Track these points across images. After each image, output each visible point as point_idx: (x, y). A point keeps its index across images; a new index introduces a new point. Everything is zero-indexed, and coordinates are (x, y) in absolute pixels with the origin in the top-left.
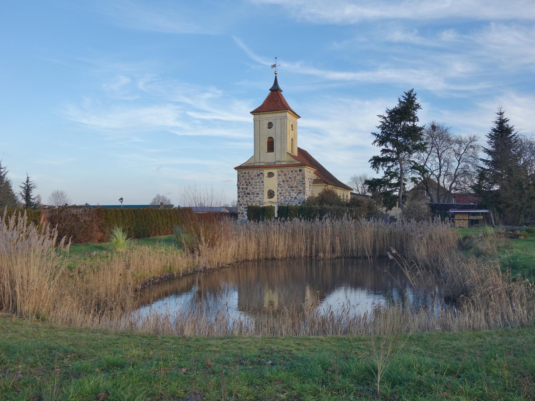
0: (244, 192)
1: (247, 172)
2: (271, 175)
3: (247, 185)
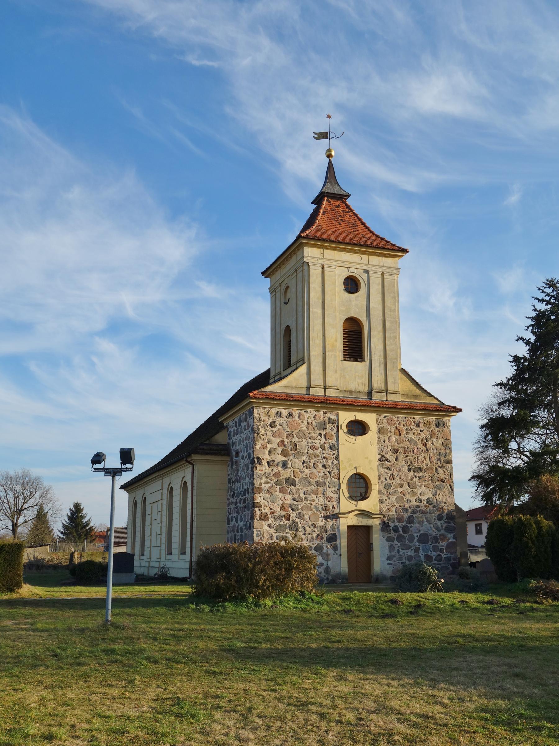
0: (277, 475)
1: (285, 412)
2: (358, 428)
3: (284, 453)
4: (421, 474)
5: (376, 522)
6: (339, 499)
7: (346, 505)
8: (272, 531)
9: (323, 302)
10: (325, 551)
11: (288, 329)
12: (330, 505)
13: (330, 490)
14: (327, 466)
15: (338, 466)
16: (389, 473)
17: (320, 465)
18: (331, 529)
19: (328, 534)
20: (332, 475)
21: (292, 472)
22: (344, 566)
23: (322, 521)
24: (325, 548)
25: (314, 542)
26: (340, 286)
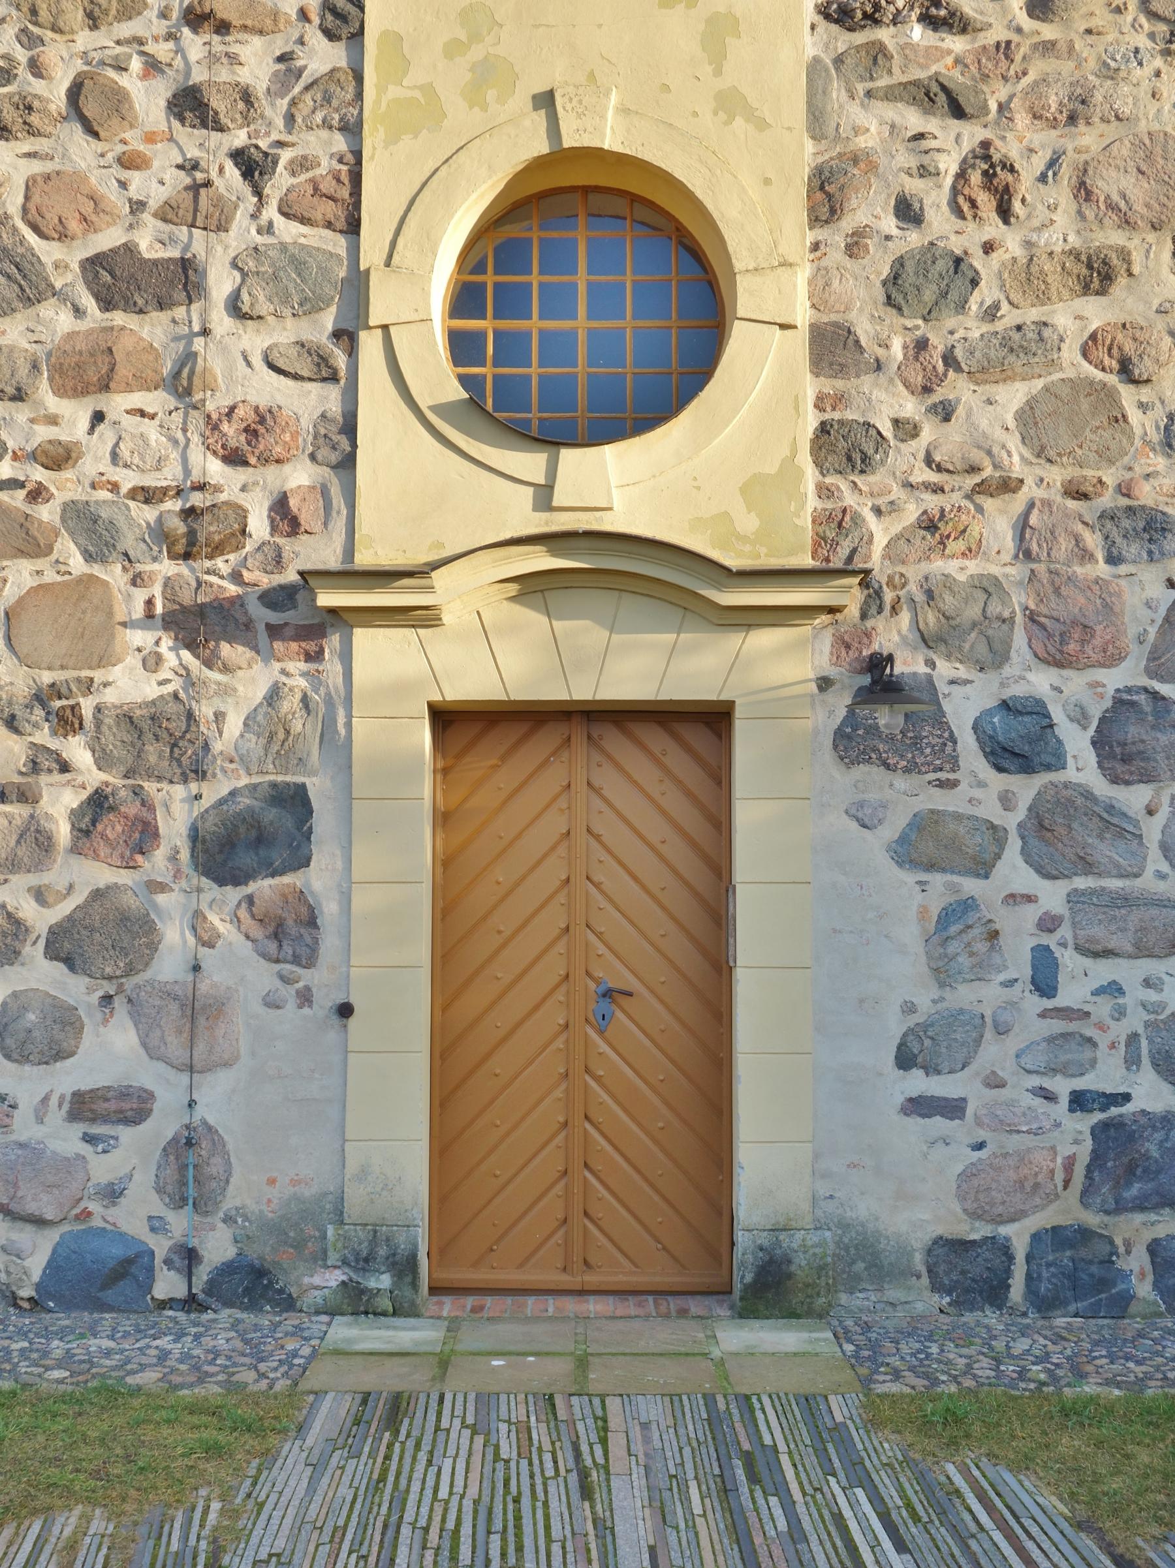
5: (776, 670)
6: (350, 428)
7: (432, 492)
10: (168, 966)
12: (249, 495)
13: (255, 341)
14: (217, 103)
16: (953, 144)
17: (149, 100)
18: (254, 744)
19: (214, 791)
20: (280, 183)
22: (390, 1157)
23: (153, 662)
24: (174, 936)
25: (54, 876)
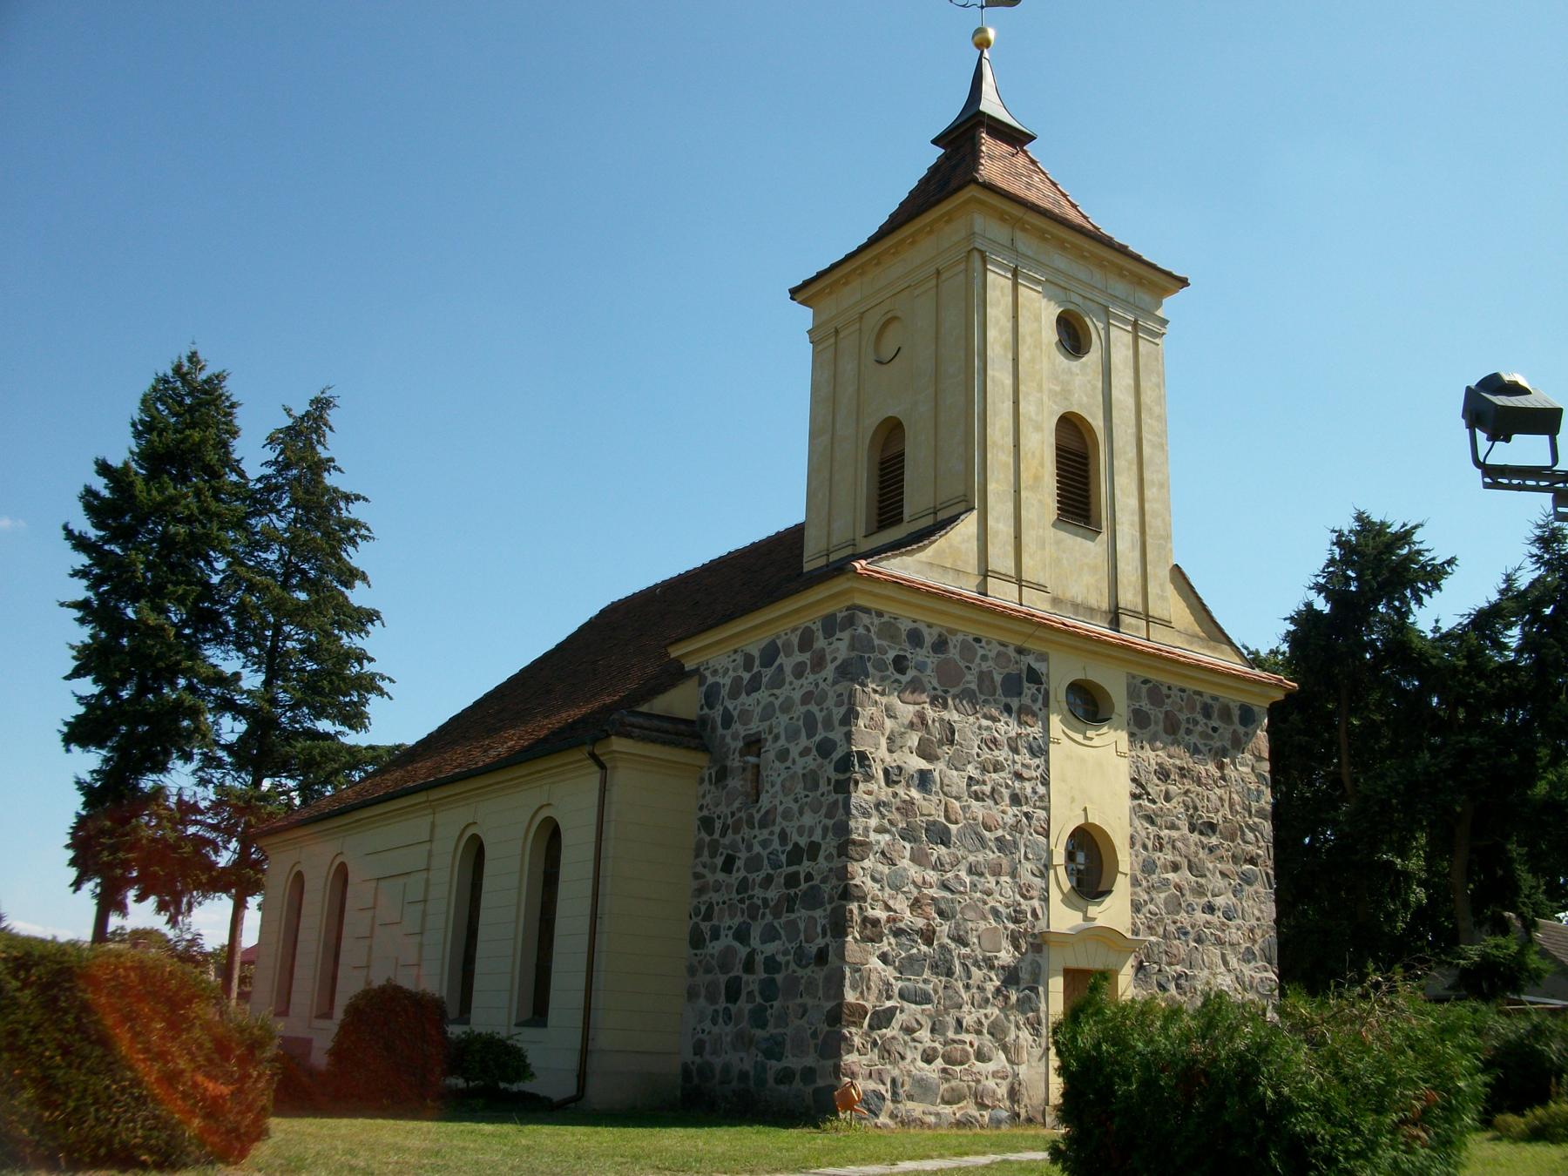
4: (1214, 840)
8: (890, 973)
9: (1015, 360)
11: (892, 431)
15: (1045, 802)
21: (942, 807)
26: (1050, 335)
